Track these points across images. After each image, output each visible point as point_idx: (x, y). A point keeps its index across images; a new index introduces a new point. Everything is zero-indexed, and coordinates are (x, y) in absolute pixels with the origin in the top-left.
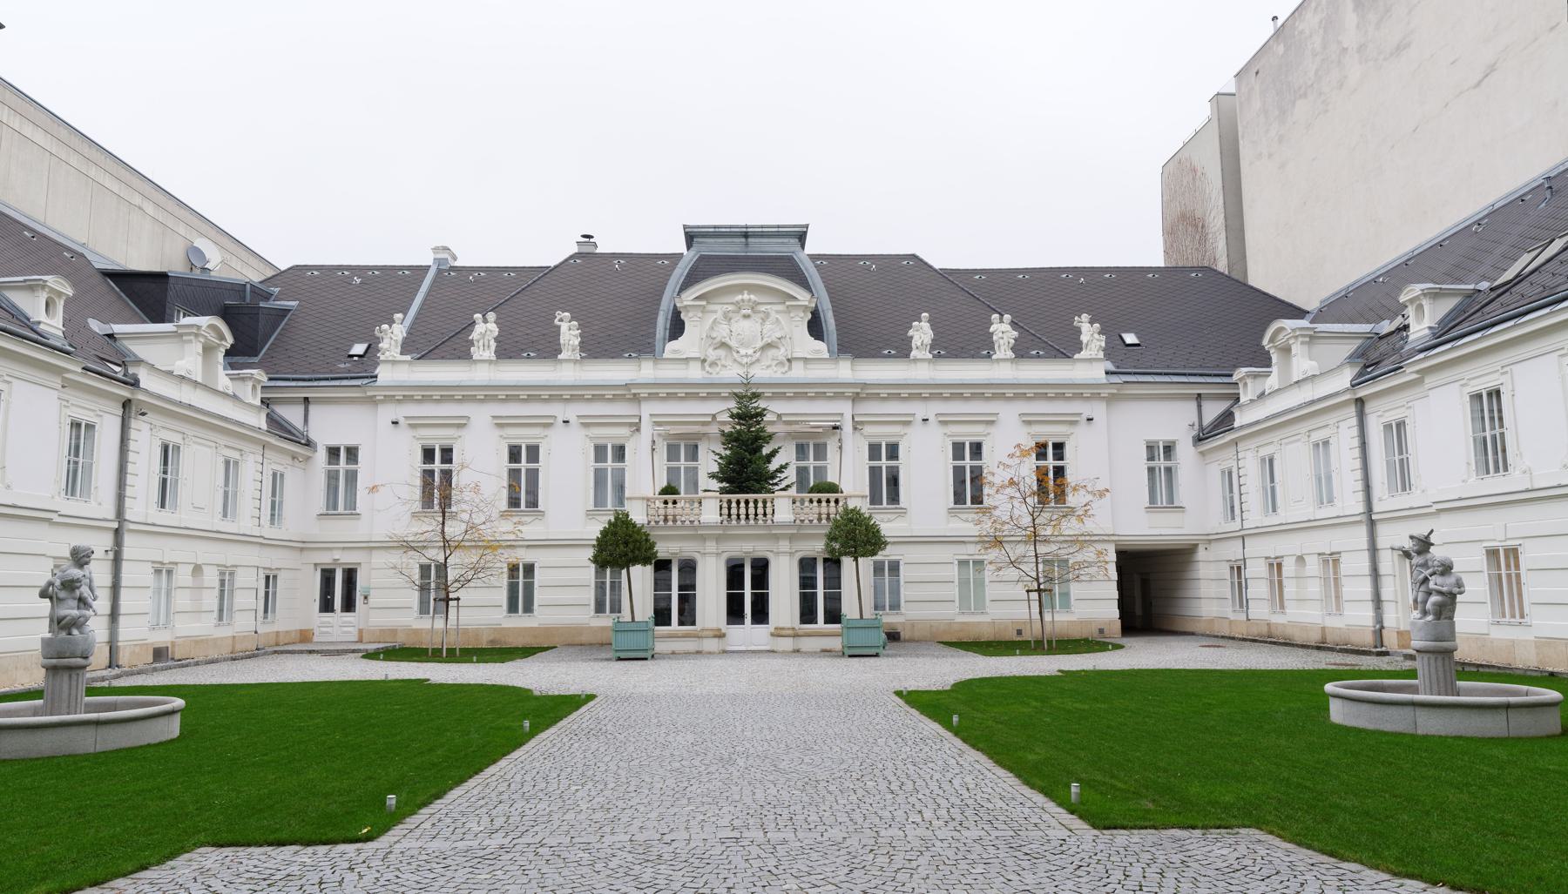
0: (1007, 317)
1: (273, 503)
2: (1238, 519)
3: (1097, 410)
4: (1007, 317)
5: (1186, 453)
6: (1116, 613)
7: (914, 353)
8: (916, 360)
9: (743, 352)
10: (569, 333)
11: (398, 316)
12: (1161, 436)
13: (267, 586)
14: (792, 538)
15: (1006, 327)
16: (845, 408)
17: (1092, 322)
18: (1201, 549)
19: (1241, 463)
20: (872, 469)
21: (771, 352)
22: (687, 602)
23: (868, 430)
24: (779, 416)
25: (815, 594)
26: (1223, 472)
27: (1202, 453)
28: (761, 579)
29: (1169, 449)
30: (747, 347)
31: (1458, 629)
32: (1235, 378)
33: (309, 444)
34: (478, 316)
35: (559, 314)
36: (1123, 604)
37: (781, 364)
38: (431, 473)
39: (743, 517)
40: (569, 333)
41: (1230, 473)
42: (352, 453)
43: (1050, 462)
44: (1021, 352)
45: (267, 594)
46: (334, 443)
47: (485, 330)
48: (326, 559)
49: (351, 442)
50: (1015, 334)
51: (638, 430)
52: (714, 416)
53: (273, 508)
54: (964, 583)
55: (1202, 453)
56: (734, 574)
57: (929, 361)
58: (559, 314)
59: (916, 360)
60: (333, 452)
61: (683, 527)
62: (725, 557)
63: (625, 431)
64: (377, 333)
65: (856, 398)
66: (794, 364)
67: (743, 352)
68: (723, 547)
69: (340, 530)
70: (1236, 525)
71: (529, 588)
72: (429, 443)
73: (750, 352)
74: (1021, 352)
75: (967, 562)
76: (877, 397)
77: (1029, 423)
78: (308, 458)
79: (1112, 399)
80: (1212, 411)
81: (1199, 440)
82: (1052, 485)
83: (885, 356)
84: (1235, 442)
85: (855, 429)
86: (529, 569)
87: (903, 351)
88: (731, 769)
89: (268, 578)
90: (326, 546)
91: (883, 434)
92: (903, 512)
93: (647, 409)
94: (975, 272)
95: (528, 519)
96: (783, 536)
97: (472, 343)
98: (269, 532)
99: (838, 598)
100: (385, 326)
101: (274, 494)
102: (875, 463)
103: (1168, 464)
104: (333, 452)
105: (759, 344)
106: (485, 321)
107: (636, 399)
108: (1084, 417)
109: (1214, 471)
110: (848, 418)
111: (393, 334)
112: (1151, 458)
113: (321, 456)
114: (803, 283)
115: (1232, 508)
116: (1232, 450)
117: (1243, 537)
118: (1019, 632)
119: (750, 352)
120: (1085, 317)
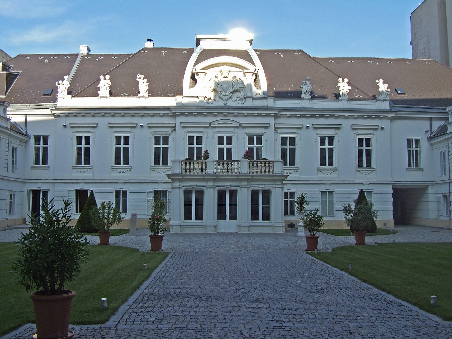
0: (108, 77)
1: (13, 161)
2: (447, 174)
3: (385, 123)
4: (346, 80)
5: (424, 144)
6: (392, 217)
7: (303, 95)
8: (304, 99)
9: (224, 94)
10: (143, 85)
11: (66, 77)
12: (414, 136)
13: (11, 199)
14: (248, 181)
15: (345, 84)
16: (271, 120)
17: (384, 83)
18: (430, 187)
19: (450, 149)
20: (190, 149)
21: (237, 94)
22: (233, 211)
23: (280, 131)
24: (240, 124)
25: (258, 207)
26: (441, 153)
27: (431, 144)
28: (267, 200)
29: (417, 141)
30: (226, 91)
31: (19, 218)
32: (447, 110)
33: (26, 135)
34: (102, 77)
35: (139, 76)
36: (395, 213)
37: (241, 99)
38: (324, 150)
39: (267, 171)
40: (143, 85)
41: (444, 153)
42: (46, 140)
43: (161, 146)
44: (152, 93)
45: (11, 202)
46: (38, 134)
47: (105, 84)
48: (35, 187)
49: (45, 134)
50: (350, 88)
51: (175, 130)
52: (210, 124)
53: (13, 164)
54: (324, 203)
55: (431, 144)
56: (221, 195)
57: (310, 99)
58: (139, 76)
59: (304, 99)
60: (38, 139)
61: (232, 175)
62: (183, 188)
63: (169, 130)
64: (57, 84)
65: (276, 117)
66: (247, 99)
67: (224, 94)
68: (217, 184)
69: (41, 173)
70: (447, 177)
71: (125, 202)
72: (80, 135)
73: (227, 94)
74: (152, 93)
75: (326, 193)
76: (285, 116)
77: (111, 127)
78: (27, 141)
79: (392, 119)
80: (437, 125)
81: (430, 138)
82: (364, 158)
83: (122, 96)
84: (447, 140)
85: (275, 130)
86: (125, 193)
87: (135, 93)
88: (256, 291)
89: (11, 195)
90: (35, 181)
91: (288, 133)
92: (297, 169)
93: (179, 120)
94: (329, 59)
95: (85, 170)
96: (177, 180)
97: (99, 89)
98: (11, 175)
99: (269, 208)
100: (60, 82)
101: (13, 158)
102: (191, 146)
103: (417, 149)
104: (38, 139)
105: (231, 90)
106: (105, 79)
107: (174, 116)
108: (380, 126)
109: (437, 152)
110: (272, 124)
111: (63, 86)
112: (409, 145)
113: (32, 140)
114: (252, 62)
115: (445, 169)
116: (446, 143)
117: (450, 183)
118: (385, 225)
119: (227, 94)
120: (381, 81)
